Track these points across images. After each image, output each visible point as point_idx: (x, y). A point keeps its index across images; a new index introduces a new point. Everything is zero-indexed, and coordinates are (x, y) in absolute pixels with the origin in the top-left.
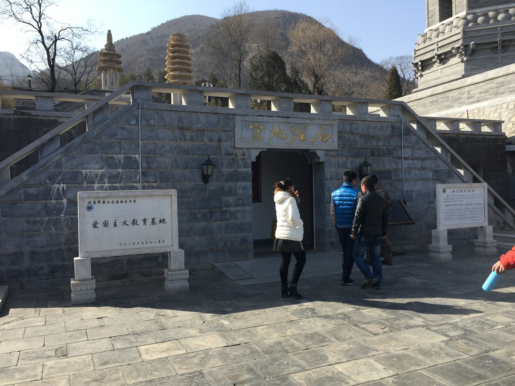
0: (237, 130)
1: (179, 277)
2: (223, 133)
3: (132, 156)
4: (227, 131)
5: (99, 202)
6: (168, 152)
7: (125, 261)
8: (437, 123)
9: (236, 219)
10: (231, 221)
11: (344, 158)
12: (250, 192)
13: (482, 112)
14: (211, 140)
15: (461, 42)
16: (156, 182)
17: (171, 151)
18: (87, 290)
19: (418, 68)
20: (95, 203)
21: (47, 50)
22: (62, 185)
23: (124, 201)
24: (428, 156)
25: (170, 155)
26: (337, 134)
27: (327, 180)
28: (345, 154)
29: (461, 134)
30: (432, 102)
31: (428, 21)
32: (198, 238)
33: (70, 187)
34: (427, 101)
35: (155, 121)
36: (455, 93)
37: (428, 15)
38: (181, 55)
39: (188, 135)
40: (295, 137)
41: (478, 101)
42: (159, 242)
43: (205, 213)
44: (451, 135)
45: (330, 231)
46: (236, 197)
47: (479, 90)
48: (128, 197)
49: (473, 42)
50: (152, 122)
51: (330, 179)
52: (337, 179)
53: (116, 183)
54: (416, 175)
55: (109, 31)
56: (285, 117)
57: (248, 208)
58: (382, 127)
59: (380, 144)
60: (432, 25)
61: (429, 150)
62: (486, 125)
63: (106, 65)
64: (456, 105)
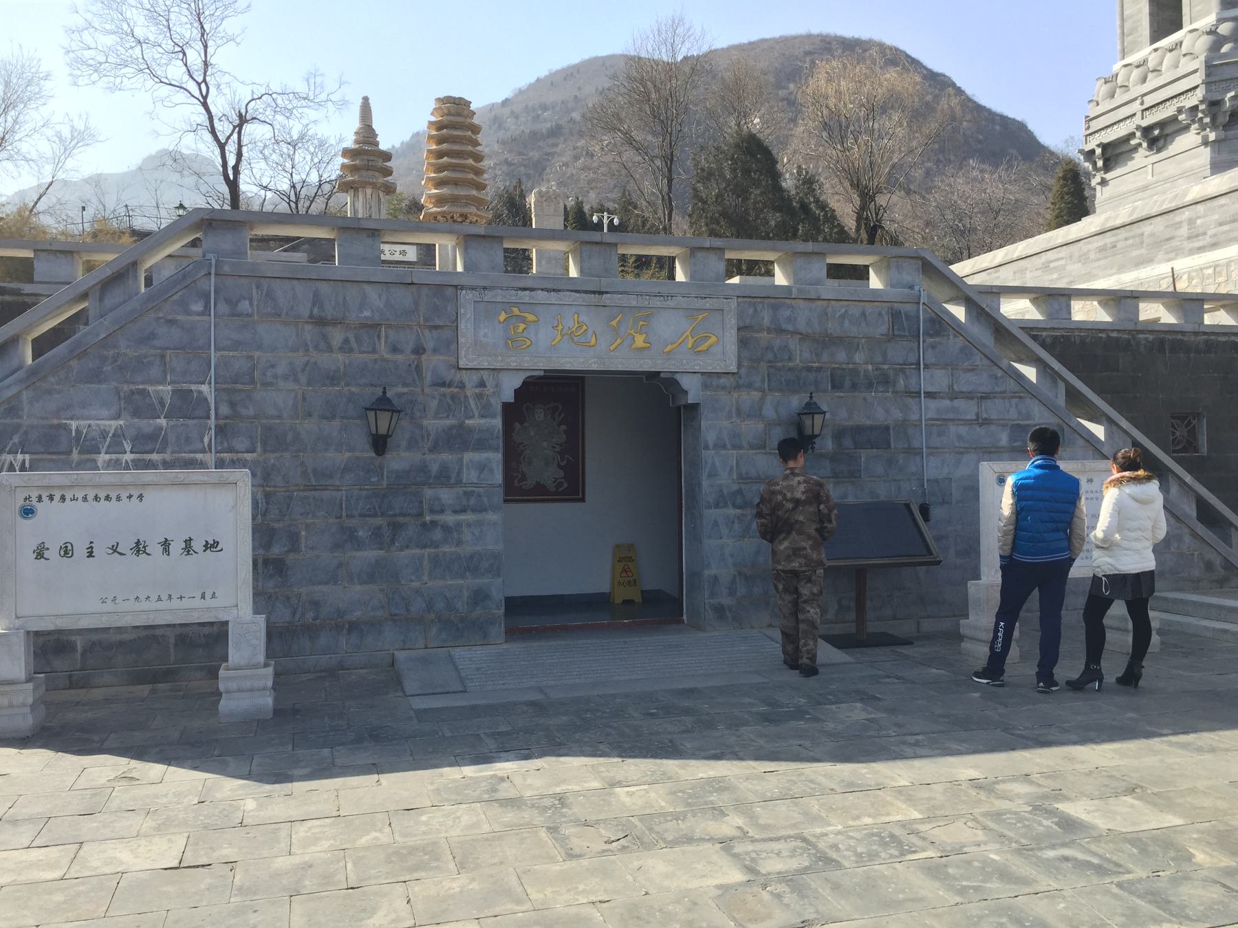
0: (462, 326)
1: (248, 684)
2: (427, 332)
3: (193, 387)
4: (436, 327)
5: (51, 498)
6: (286, 378)
7: (172, 640)
8: (1142, 306)
9: (459, 543)
10: (447, 549)
11: (756, 395)
12: (498, 477)
13: (1224, 273)
14: (395, 349)
15: (1200, 93)
16: (253, 451)
17: (292, 375)
18: (11, 706)
19: (1095, 164)
20: (40, 499)
21: (222, 147)
22: (20, 457)
23: (113, 495)
24: (997, 389)
25: (291, 385)
26: (734, 332)
27: (707, 448)
28: (757, 385)
29: (1142, 332)
30: (1102, 249)
31: (1123, 42)
32: (358, 588)
33: (40, 460)
34: (1090, 246)
35: (251, 304)
36: (1157, 226)
37: (1122, 27)
38: (456, 147)
39: (337, 336)
40: (619, 341)
41: (1215, 245)
42: (203, 597)
43: (379, 528)
44: (1114, 335)
45: (716, 578)
46: (460, 490)
47: (1216, 217)
48: (124, 486)
49: (1233, 94)
50: (244, 306)
51: (716, 446)
52: (734, 447)
53: (151, 452)
54: (960, 437)
55: (366, 99)
56: (594, 292)
57: (491, 516)
58: (864, 314)
59: (859, 357)
60: (1132, 51)
61: (1000, 373)
62: (1223, 307)
63: (356, 178)
64: (1160, 256)
